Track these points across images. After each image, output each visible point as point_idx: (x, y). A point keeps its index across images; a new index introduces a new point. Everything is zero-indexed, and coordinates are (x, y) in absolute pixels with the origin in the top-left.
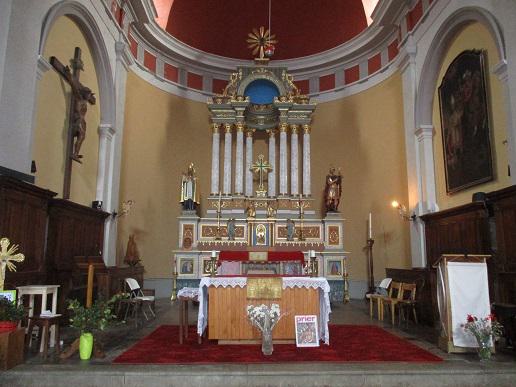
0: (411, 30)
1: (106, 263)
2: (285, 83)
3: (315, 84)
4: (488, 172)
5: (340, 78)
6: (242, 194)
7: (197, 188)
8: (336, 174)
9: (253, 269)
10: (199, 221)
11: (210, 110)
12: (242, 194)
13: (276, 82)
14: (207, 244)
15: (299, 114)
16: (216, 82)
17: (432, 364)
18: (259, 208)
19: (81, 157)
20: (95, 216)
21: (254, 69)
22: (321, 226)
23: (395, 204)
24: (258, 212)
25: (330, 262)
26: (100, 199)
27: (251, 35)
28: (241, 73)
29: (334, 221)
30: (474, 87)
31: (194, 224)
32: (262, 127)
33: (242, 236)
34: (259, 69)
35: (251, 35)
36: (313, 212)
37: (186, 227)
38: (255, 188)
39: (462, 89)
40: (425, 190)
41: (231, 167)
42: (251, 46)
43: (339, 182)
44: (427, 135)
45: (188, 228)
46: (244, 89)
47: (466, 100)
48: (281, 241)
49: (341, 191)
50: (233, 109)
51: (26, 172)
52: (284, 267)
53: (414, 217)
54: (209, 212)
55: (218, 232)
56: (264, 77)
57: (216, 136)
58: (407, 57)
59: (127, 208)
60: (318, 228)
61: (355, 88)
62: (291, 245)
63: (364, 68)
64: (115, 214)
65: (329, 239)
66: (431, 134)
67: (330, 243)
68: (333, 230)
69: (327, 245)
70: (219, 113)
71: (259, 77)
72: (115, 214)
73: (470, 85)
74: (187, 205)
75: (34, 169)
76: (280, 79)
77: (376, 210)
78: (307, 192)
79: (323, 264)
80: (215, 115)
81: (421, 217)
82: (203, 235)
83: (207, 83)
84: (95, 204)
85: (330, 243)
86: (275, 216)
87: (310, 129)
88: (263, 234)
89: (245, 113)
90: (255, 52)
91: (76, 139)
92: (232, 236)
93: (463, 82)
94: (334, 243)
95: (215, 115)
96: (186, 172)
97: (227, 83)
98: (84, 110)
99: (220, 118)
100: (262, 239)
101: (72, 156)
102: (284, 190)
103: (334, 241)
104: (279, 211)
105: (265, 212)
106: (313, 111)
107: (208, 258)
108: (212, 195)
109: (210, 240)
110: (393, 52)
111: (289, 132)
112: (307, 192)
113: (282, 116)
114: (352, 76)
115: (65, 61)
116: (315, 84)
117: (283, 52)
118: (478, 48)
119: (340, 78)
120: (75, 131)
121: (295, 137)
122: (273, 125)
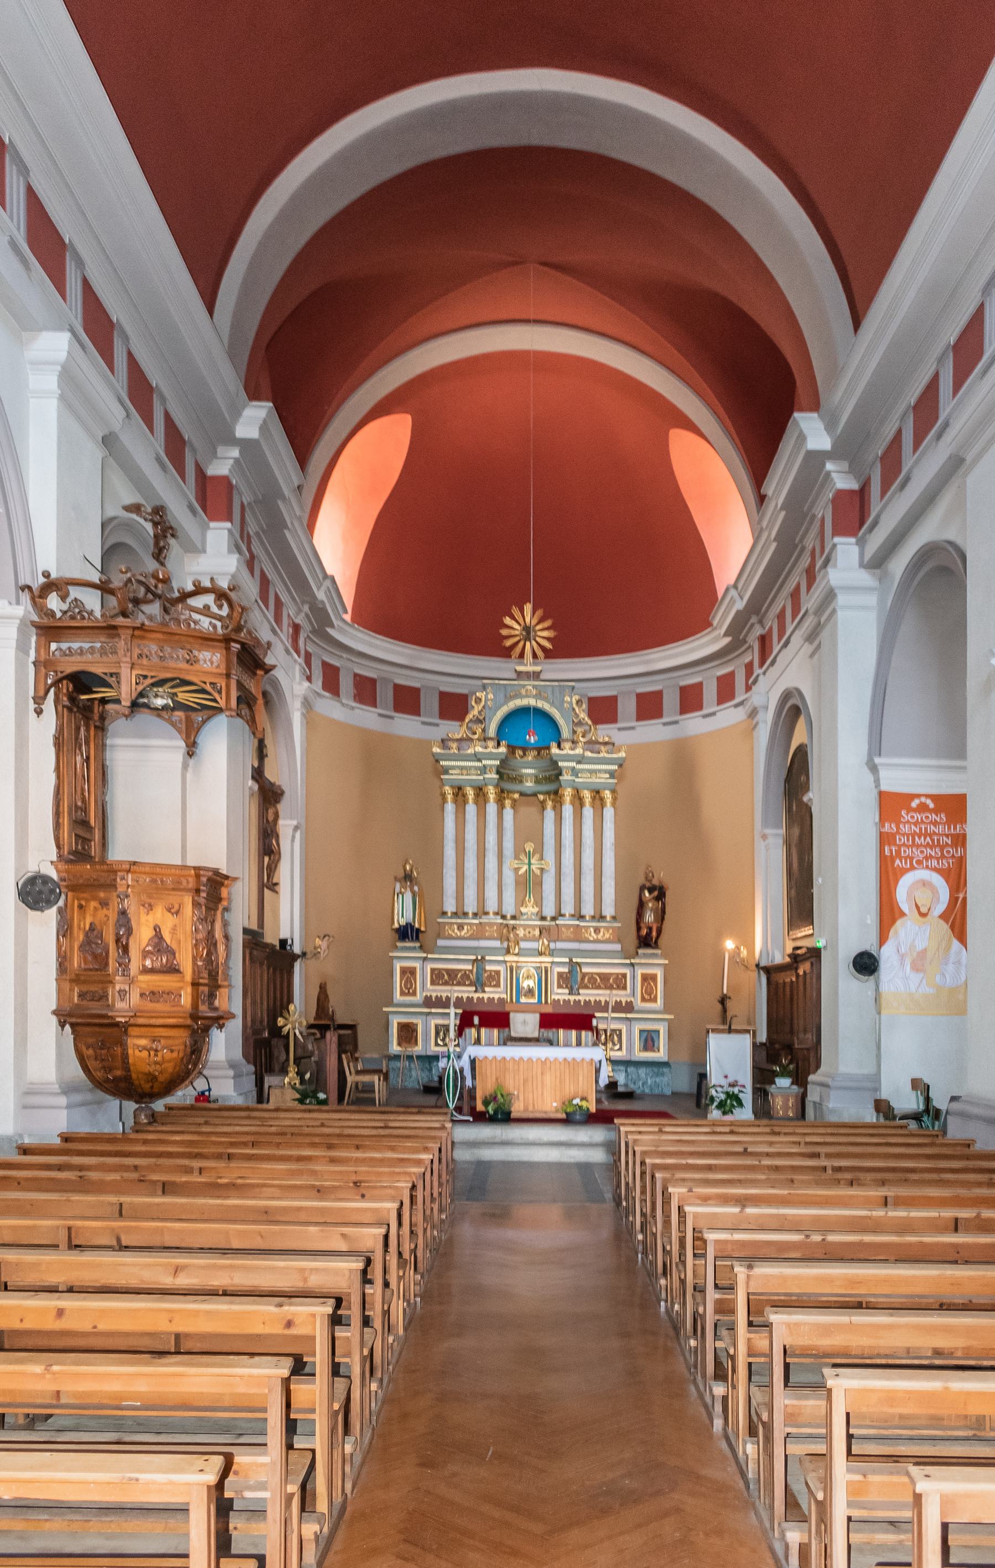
6: (497, 914)
9: (705, 1200)
12: (497, 914)
14: (439, 999)
15: (595, 771)
16: (444, 696)
18: (525, 939)
24: (523, 945)
27: (508, 621)
29: (653, 964)
31: (417, 965)
35: (508, 621)
36: (618, 947)
37: (404, 971)
48: (560, 995)
49: (663, 912)
54: (441, 943)
55: (451, 977)
56: (532, 702)
57: (450, 807)
60: (624, 976)
61: (694, 724)
64: (304, 954)
67: (643, 1000)
69: (638, 1004)
70: (453, 768)
74: (406, 933)
78: (609, 911)
80: (446, 771)
82: (433, 983)
85: (643, 1000)
86: (552, 953)
87: (615, 799)
91: (266, 859)
92: (479, 984)
94: (409, 994)
95: (446, 771)
96: (402, 874)
99: (454, 776)
100: (530, 992)
103: (649, 996)
104: (560, 945)
105: (534, 945)
106: (620, 766)
109: (442, 991)
111: (578, 800)
112: (609, 911)
113: (565, 777)
114: (690, 700)
117: (565, 646)
121: (588, 812)
122: (551, 787)
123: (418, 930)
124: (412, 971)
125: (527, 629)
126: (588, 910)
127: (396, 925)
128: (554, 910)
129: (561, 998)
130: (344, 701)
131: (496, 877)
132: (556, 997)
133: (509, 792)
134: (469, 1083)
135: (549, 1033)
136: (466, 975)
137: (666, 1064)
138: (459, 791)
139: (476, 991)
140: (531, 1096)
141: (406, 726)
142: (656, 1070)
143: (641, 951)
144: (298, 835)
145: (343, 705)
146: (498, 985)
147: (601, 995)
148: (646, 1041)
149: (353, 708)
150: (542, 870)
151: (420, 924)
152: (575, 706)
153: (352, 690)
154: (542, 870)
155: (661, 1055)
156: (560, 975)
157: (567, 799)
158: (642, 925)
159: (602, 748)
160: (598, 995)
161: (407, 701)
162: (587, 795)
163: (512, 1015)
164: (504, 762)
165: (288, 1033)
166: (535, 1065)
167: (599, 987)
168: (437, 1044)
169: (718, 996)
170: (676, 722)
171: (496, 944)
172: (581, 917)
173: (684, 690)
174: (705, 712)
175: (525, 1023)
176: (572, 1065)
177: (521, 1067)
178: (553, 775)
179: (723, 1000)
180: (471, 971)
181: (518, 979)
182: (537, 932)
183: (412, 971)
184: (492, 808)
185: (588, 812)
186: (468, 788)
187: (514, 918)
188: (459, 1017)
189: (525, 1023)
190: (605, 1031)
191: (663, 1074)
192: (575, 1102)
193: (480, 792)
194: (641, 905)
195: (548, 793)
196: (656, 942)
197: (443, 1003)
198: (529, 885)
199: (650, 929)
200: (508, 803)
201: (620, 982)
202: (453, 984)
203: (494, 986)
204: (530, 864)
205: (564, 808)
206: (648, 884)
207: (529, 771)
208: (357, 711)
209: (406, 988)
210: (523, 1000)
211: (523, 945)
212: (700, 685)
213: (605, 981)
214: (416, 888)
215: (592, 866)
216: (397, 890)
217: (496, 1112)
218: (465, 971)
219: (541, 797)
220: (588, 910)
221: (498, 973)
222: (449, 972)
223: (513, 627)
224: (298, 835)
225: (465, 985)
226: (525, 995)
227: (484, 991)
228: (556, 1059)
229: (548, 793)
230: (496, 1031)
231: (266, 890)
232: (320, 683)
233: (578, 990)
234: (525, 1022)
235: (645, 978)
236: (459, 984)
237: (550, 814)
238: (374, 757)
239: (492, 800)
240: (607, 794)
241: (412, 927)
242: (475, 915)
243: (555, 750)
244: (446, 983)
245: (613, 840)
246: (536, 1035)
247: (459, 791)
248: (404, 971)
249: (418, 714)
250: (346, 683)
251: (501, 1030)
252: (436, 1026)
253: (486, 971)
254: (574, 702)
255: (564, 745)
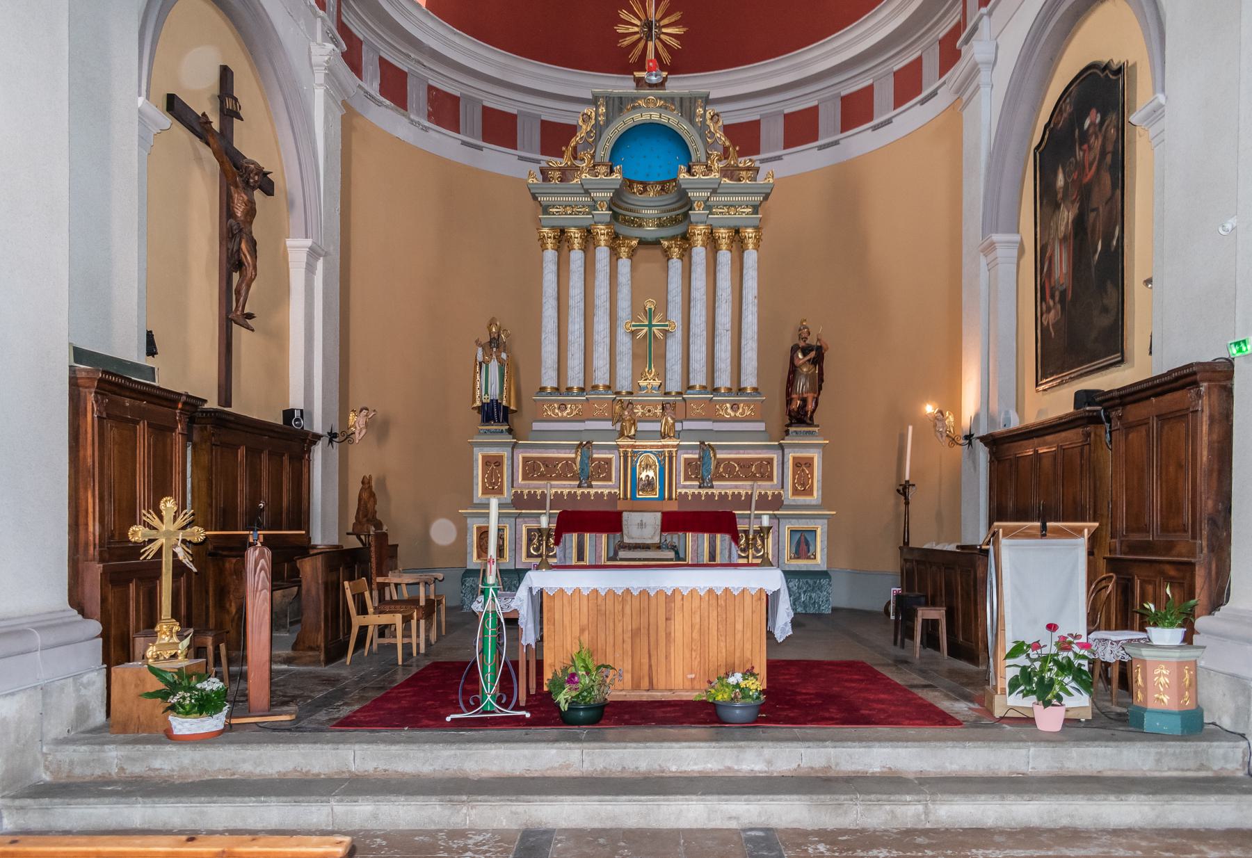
0: (986, 4)
1: (697, 456)
2: (703, 130)
3: (773, 132)
4: (1112, 344)
5: (830, 117)
6: (608, 388)
7: (510, 371)
8: (812, 341)
10: (514, 446)
11: (535, 197)
13: (683, 127)
16: (546, 126)
17: (928, 731)
19: (250, 316)
20: (288, 440)
21: (634, 99)
22: (775, 456)
23: (929, 409)
24: (641, 426)
25: (792, 532)
26: (296, 401)
27: (624, 14)
28: (602, 110)
30: (1103, 153)
32: (653, 225)
33: (609, 478)
34: (644, 97)
36: (761, 426)
37: (487, 461)
38: (638, 374)
39: (1079, 154)
40: (989, 380)
41: (585, 319)
42: (673, 18)
43: (818, 360)
44: (1005, 254)
45: (493, 464)
46: (609, 146)
47: (1086, 180)
48: (687, 488)
49: (821, 380)
50: (587, 192)
51: (135, 360)
52: (695, 543)
53: (969, 437)
54: (537, 426)
56: (655, 117)
57: (550, 255)
58: (974, 71)
59: (356, 421)
61: (862, 141)
62: (710, 497)
63: (884, 94)
65: (799, 485)
66: (1015, 253)
67: (796, 492)
68: (803, 465)
69: (788, 496)
71: (646, 117)
72: (332, 436)
73: (1097, 143)
74: (493, 413)
75: (151, 350)
76: (691, 121)
77: (899, 418)
78: (749, 381)
79: (780, 542)
81: (982, 439)
83: (529, 134)
84: (288, 414)
85: (796, 492)
86: (678, 435)
87: (758, 240)
88: (651, 474)
89: (613, 204)
90: (634, 57)
91: (236, 276)
92: (585, 478)
93: (1084, 137)
95: (545, 209)
96: (486, 339)
97: (573, 130)
98: (251, 212)
99: (558, 217)
100: (649, 484)
101: (233, 316)
102: (699, 379)
103: (803, 487)
104: (688, 425)
105: (656, 426)
107: (534, 525)
108: (543, 389)
110: (950, 54)
111: (712, 242)
112: (749, 381)
113: (698, 212)
114: (857, 110)
115: (204, 104)
116: (773, 132)
118: (1117, 61)
119: (830, 117)
120: (238, 253)
121: (725, 257)
122: (677, 230)
123: (506, 409)
124: (498, 462)
125: (648, 25)
126: (723, 381)
127: (478, 403)
128: (679, 384)
129: (690, 491)
130: (412, 117)
131: (607, 340)
132: (683, 491)
133: (626, 238)
134: (528, 637)
135: (673, 538)
136: (568, 463)
137: (824, 574)
138: (562, 236)
139: (579, 486)
140: (645, 660)
141: (497, 161)
142: (811, 582)
143: (792, 429)
144: (320, 265)
145: (412, 122)
146: (609, 478)
147: (742, 487)
148: (799, 543)
149: (426, 129)
150: (665, 332)
151: (509, 401)
152: (708, 122)
153: (425, 107)
154: (665, 332)
155: (819, 561)
156: (688, 463)
157: (699, 240)
158: (794, 396)
159: (743, 174)
160: (736, 487)
161: (499, 129)
162: (723, 233)
163: (625, 515)
164: (618, 194)
165: (159, 553)
166: (653, 602)
167: (737, 478)
168: (529, 555)
169: (892, 483)
170: (836, 143)
171: (608, 425)
172: (716, 390)
173: (846, 101)
174: (875, 122)
175: (642, 526)
176: (724, 601)
177: (628, 609)
178: (681, 210)
179: (904, 490)
180: (574, 460)
181: (634, 469)
182: (659, 411)
183: (498, 462)
184: (602, 253)
185: (725, 257)
186: (573, 230)
187: (630, 393)
188: (556, 520)
189: (642, 526)
190: (746, 532)
191: (820, 588)
192: (732, 680)
193: (589, 236)
194: (793, 370)
195: (673, 238)
196: (811, 417)
197: (536, 502)
198: (649, 351)
199: (804, 401)
200: (624, 251)
201: (762, 471)
202: (551, 479)
203: (604, 479)
204: (650, 326)
205: (695, 250)
206: (802, 344)
207: (650, 209)
208: (431, 133)
209: (491, 484)
210: (641, 495)
211: (641, 426)
212: (869, 90)
213: (747, 470)
214: (504, 356)
215: (728, 326)
216: (480, 358)
217: (573, 706)
218: (567, 459)
219: (666, 243)
220: (723, 381)
221: (608, 462)
222: (546, 461)
223: (630, 27)
224: (320, 265)
225: (566, 478)
226: (643, 490)
227: (590, 486)
228: (693, 591)
229: (673, 238)
230: (604, 536)
231: (234, 325)
232: (376, 85)
233: (711, 481)
234: (642, 525)
235: (798, 463)
236: (559, 478)
237: (676, 265)
238: (455, 192)
239: (603, 243)
240: (749, 232)
241: (499, 405)
242: (582, 390)
243: (683, 176)
244: (542, 477)
245: (755, 292)
246: (656, 540)
247: (562, 236)
248: (926, 622)
249: (514, 146)
250: (417, 95)
251: (611, 536)
252: (529, 531)
253: (593, 460)
254: (708, 116)
255: (696, 169)
